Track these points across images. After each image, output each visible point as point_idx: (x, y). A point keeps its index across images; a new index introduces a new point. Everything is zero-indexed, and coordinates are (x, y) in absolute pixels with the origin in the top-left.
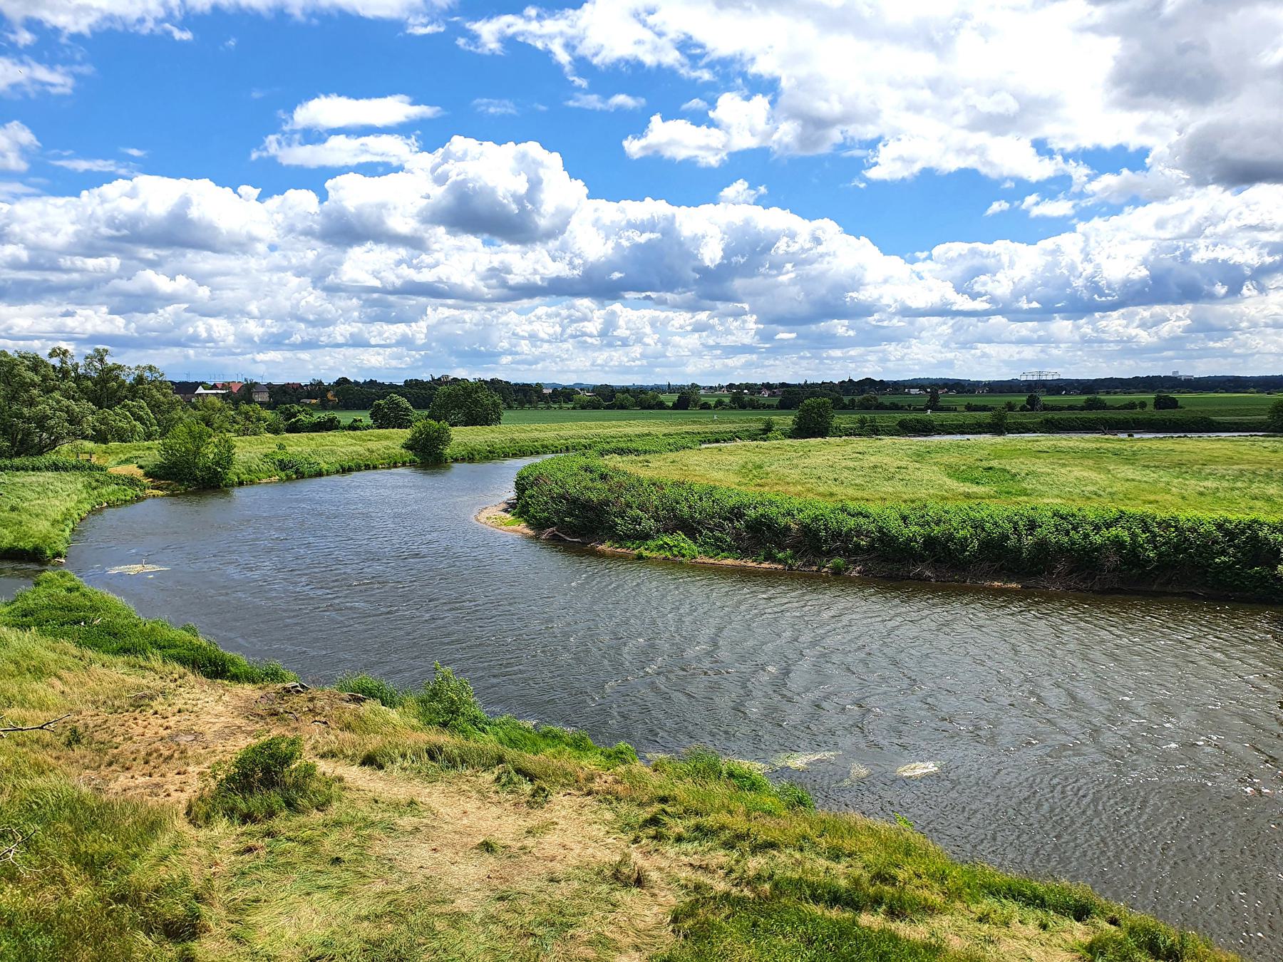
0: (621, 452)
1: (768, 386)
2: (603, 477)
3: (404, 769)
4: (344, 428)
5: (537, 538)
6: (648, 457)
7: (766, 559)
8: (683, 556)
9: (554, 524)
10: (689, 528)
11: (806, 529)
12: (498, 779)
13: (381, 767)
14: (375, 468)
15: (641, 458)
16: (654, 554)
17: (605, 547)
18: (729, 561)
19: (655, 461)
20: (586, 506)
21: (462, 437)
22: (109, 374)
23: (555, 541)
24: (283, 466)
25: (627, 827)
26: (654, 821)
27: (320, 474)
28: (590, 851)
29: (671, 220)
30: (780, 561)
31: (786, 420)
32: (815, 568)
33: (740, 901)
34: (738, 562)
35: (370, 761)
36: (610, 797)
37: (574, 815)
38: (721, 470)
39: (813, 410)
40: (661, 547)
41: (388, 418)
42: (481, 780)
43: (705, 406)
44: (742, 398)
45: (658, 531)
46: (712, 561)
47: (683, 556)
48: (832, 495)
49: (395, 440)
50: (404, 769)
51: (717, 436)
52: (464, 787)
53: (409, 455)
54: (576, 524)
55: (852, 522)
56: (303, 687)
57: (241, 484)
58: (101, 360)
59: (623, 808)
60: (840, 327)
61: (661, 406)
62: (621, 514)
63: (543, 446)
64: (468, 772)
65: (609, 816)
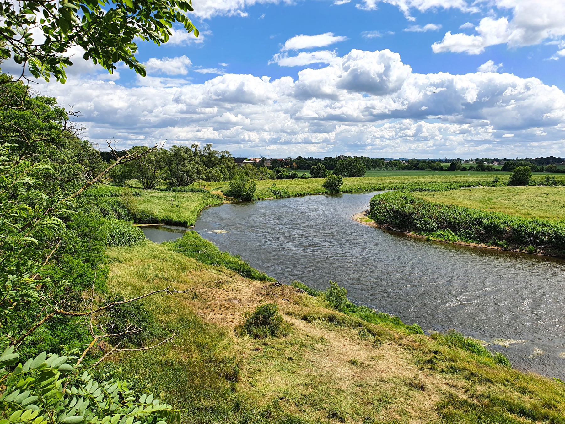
0: (421, 190)
1: (497, 160)
2: (412, 202)
3: (319, 324)
4: (299, 178)
5: (379, 228)
6: (433, 193)
7: (492, 245)
8: (450, 240)
9: (387, 222)
10: (454, 227)
11: (514, 231)
12: (359, 333)
13: (310, 322)
14: (311, 194)
15: (431, 193)
16: (435, 239)
17: (412, 234)
18: (473, 244)
19: (438, 195)
20: (403, 215)
21: (348, 182)
22: (211, 154)
23: (388, 230)
24: (275, 193)
25: (418, 362)
26: (430, 361)
27: (289, 197)
28: (400, 370)
29: (451, 82)
30: (500, 246)
31: (506, 177)
32: (518, 250)
33: (473, 406)
34: (478, 245)
35: (305, 318)
36: (409, 348)
37: (393, 354)
38: (471, 200)
39: (519, 173)
40: (439, 236)
41: (316, 174)
42: (352, 333)
43: (464, 169)
44: (482, 166)
45: (438, 228)
46: (464, 244)
47: (450, 240)
48: (529, 214)
49: (319, 183)
50: (319, 324)
51: (469, 184)
52: (344, 335)
53: (324, 189)
54: (398, 223)
55: (539, 229)
56: (280, 284)
57: (259, 199)
58: (209, 149)
59: (416, 353)
60: (538, 131)
61: (441, 169)
62: (420, 219)
63: (383, 187)
64: (346, 328)
65: (409, 356)
